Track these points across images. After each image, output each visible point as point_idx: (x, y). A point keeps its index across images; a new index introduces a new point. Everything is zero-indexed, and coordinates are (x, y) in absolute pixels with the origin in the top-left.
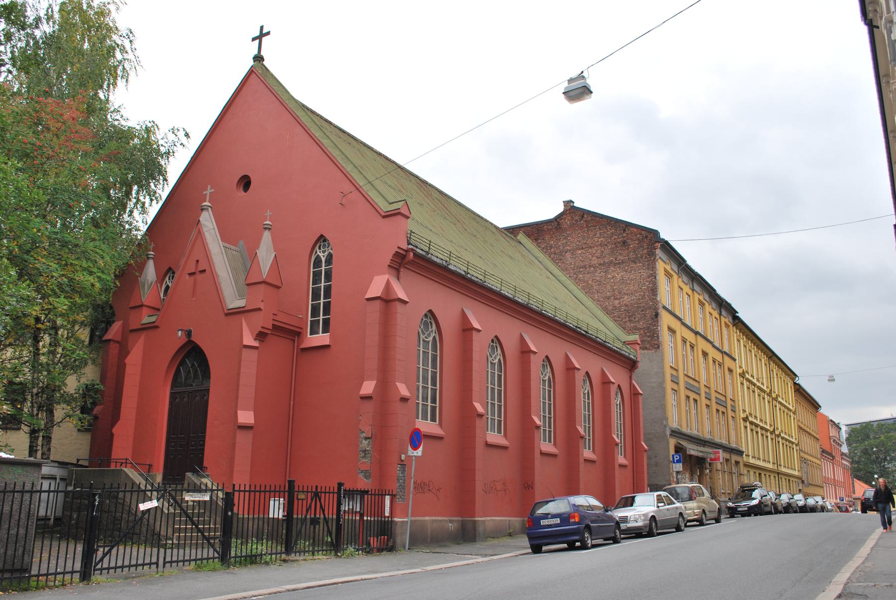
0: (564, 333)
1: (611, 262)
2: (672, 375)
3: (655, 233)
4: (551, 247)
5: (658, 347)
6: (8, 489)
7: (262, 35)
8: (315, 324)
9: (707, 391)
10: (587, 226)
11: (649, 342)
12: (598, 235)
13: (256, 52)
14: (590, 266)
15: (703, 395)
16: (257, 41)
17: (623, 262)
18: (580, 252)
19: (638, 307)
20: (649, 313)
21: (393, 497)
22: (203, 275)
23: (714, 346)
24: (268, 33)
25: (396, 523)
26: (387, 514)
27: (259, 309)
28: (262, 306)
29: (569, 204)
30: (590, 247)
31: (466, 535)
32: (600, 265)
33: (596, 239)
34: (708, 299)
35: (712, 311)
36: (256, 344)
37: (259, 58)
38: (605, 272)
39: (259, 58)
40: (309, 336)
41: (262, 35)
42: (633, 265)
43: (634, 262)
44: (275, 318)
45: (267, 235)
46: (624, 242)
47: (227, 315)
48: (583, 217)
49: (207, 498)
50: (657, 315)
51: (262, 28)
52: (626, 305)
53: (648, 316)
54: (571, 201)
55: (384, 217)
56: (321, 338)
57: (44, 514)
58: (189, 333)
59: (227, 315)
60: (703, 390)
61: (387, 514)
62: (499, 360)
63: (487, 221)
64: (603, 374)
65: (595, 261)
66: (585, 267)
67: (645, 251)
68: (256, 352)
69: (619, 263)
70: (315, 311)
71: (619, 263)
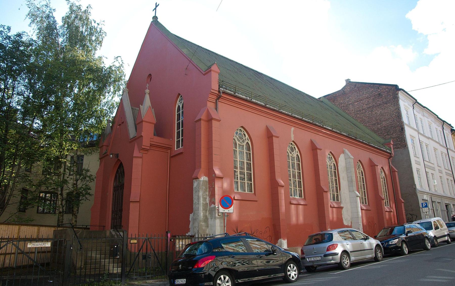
0: (381, 153)
1: (374, 105)
2: (416, 161)
4: (341, 104)
5: (406, 146)
6: (7, 252)
9: (439, 168)
11: (400, 144)
14: (363, 110)
15: (437, 171)
17: (380, 105)
18: (356, 103)
19: (391, 127)
23: (441, 145)
29: (348, 81)
30: (362, 100)
32: (368, 108)
34: (434, 121)
35: (437, 127)
38: (371, 111)
39: (155, 18)
42: (385, 105)
43: (387, 104)
44: (152, 140)
47: (130, 142)
48: (356, 86)
52: (385, 127)
53: (398, 130)
54: (349, 79)
57: (80, 266)
58: (117, 156)
59: (130, 142)
60: (437, 168)
61: (48, 245)
62: (297, 155)
63: (232, 61)
64: (370, 161)
65: (365, 106)
66: (360, 111)
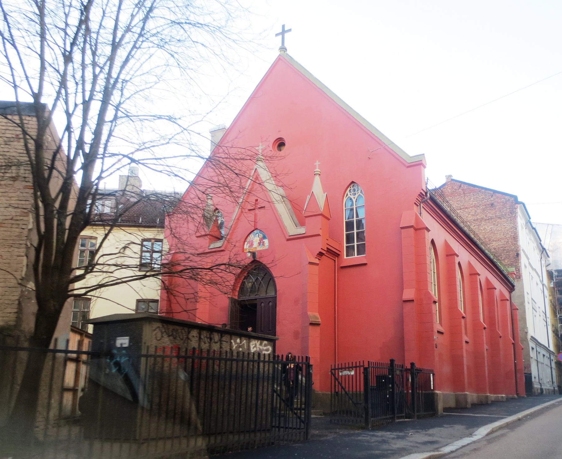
1: (482, 219)
3: (515, 198)
5: (520, 278)
7: (284, 32)
8: (350, 250)
10: (464, 193)
12: (472, 199)
13: (280, 45)
16: (281, 36)
17: (491, 219)
19: (504, 250)
20: (512, 254)
21: (433, 375)
22: (262, 210)
24: (290, 30)
25: (437, 394)
26: (432, 388)
27: (319, 235)
28: (320, 232)
30: (466, 208)
31: (520, 398)
32: (474, 220)
33: (471, 203)
36: (317, 261)
37: (283, 49)
39: (283, 49)
40: (345, 257)
41: (284, 32)
43: (500, 218)
44: (327, 242)
45: (317, 178)
46: (492, 204)
47: (288, 240)
48: (460, 186)
49: (353, 373)
50: (518, 255)
51: (283, 26)
53: (511, 256)
54: (450, 176)
55: (408, 167)
56: (356, 258)
59: (288, 240)
67: (509, 210)
68: (316, 267)
69: (488, 219)
70: (349, 239)
71: (488, 219)
